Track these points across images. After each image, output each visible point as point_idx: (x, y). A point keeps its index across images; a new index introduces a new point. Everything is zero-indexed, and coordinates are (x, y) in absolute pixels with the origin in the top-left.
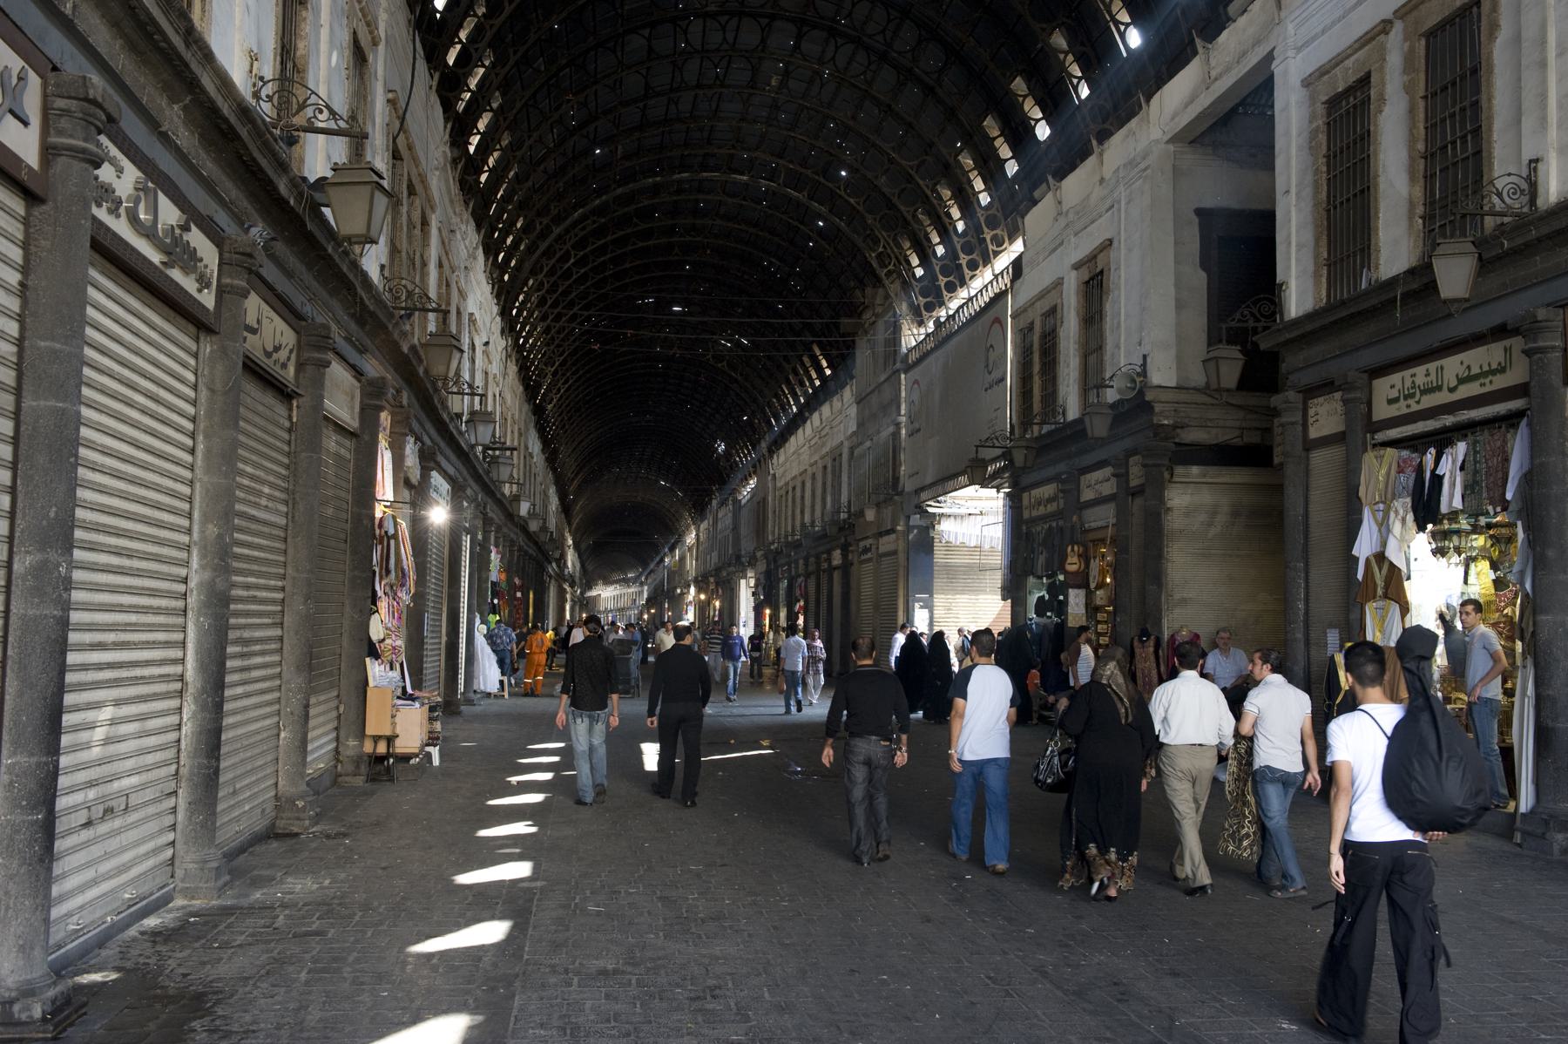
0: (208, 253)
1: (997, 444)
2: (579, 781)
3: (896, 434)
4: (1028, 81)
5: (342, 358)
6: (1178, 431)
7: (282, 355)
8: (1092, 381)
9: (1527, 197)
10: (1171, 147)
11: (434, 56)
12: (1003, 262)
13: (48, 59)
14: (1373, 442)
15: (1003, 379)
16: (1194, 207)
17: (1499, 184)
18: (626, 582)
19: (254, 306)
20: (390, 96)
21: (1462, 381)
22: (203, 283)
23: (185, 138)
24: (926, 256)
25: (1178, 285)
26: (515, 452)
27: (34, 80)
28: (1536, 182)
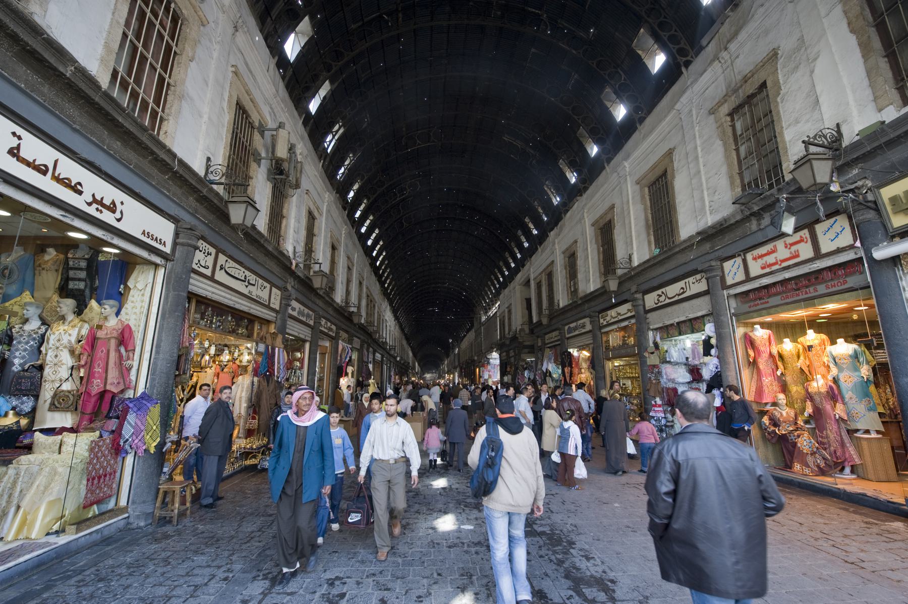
0: (334, 327)
1: (622, 267)
4: (522, 231)
5: (356, 337)
8: (510, 330)
11: (351, 216)
12: (497, 305)
13: (258, 263)
18: (433, 373)
23: (331, 312)
24: (486, 302)
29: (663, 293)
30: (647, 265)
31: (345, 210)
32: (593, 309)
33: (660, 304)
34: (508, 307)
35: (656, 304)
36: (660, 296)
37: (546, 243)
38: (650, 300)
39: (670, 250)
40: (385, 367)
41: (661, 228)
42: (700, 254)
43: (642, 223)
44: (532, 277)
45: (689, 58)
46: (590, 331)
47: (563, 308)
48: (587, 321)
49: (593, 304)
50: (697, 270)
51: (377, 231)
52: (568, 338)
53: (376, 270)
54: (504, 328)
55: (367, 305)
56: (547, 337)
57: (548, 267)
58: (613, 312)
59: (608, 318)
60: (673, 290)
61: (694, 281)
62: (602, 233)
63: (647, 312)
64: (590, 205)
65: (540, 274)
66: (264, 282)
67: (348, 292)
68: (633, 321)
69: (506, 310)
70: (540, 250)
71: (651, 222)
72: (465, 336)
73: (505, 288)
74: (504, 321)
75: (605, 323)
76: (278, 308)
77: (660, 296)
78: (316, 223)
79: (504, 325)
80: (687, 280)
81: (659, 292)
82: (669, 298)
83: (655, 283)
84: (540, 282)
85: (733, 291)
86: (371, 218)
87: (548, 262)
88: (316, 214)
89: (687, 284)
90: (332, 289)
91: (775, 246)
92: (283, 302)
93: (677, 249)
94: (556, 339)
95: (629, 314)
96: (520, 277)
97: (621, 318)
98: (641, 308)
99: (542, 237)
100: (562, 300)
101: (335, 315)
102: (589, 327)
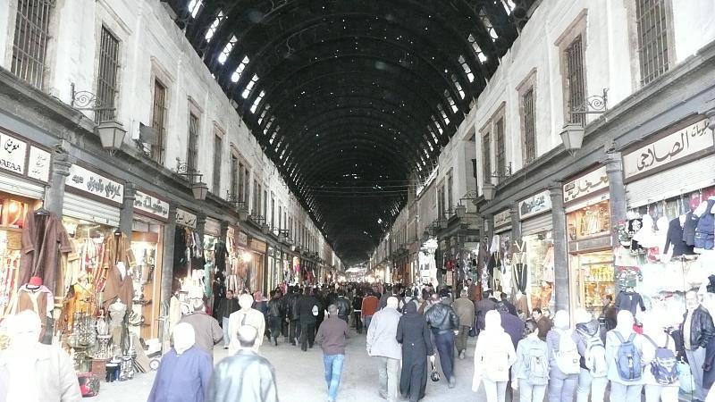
3: (416, 221)
7: (192, 222)
10: (464, 142)
17: (590, 100)
19: (180, 212)
22: (165, 213)
23: (158, 183)
25: (467, 182)
26: (48, 191)
27: (122, 186)
29: (649, 151)
30: (627, 107)
31: (182, 28)
32: (553, 178)
33: (645, 169)
34: (449, 173)
35: (640, 169)
36: (645, 156)
37: (496, 74)
38: (633, 162)
39: (658, 81)
40: (270, 258)
41: (650, 47)
42: (705, 88)
43: (625, 39)
44: (478, 128)
46: (549, 212)
48: (546, 195)
49: (555, 168)
50: (697, 113)
51: (246, 60)
52: (522, 221)
53: (249, 120)
54: (444, 203)
55: (234, 171)
56: (496, 217)
57: (497, 112)
58: (580, 182)
59: (575, 191)
60: (663, 146)
61: (695, 131)
62: (569, 56)
63: (627, 182)
64: (552, 13)
65: (488, 123)
66: (12, 139)
67: (192, 153)
68: (608, 196)
69: (447, 177)
70: (488, 85)
71: (636, 36)
72: (397, 214)
73: (444, 145)
74: (443, 194)
75: (571, 199)
76: (45, 178)
77: (645, 156)
78: (122, 49)
79: (443, 199)
80: (684, 131)
81: (644, 150)
82: (658, 160)
83: (638, 136)
85: (498, 231)
86: (234, 39)
87: (499, 103)
88: (118, 32)
89: (685, 137)
90: (159, 148)
92: (55, 169)
93: (670, 81)
94: (507, 221)
95: (603, 185)
96: (463, 129)
97: (591, 190)
98: (619, 175)
99: (491, 68)
100: (516, 161)
101: (166, 186)
102: (548, 205)
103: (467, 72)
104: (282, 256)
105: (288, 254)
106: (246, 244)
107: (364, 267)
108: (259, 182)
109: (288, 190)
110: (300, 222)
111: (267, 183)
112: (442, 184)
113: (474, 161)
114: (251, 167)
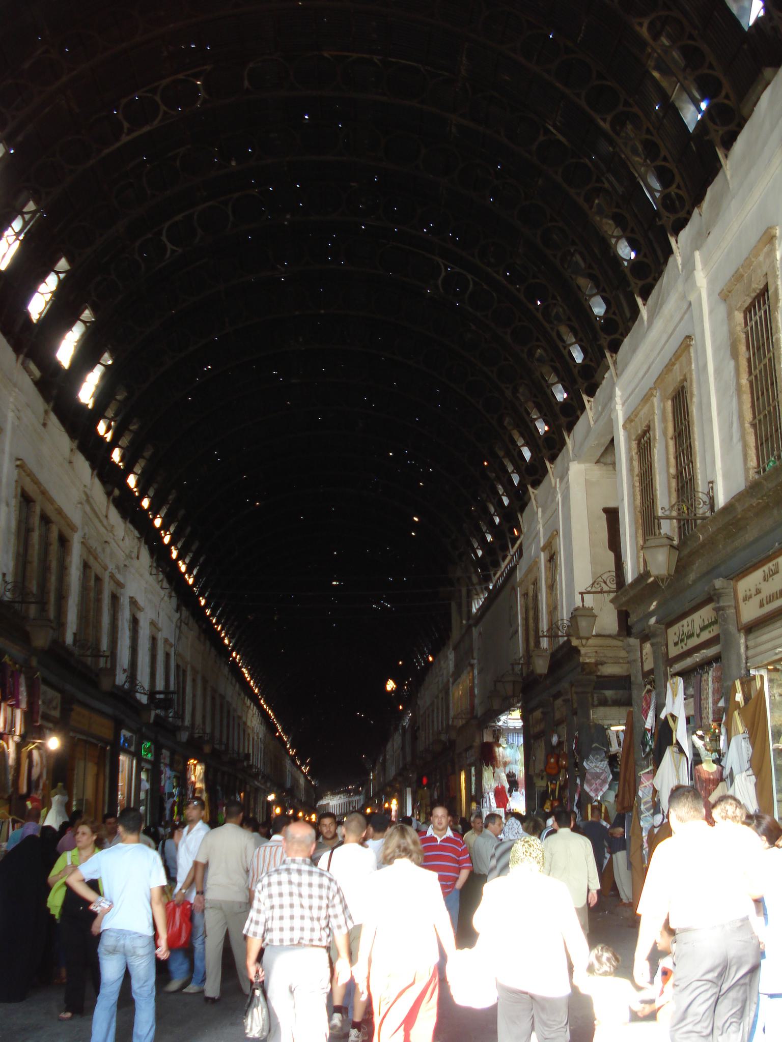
2: (96, 923)
6: (600, 667)
9: (709, 506)
14: (671, 673)
15: (517, 631)
16: (602, 507)
20: (18, 463)
21: (703, 629)
28: (713, 496)
45: (617, 336)
47: (729, 508)
52: (750, 629)
56: (673, 633)
69: (543, 557)
84: (648, 430)
85: (678, 667)
91: (777, 565)
94: (706, 636)
103: (519, 444)
104: (157, 755)
105: (173, 753)
106: (56, 714)
107: (357, 793)
108: (96, 567)
109: (174, 601)
110: (205, 681)
111: (119, 577)
112: (531, 578)
113: (612, 515)
114: (73, 529)
